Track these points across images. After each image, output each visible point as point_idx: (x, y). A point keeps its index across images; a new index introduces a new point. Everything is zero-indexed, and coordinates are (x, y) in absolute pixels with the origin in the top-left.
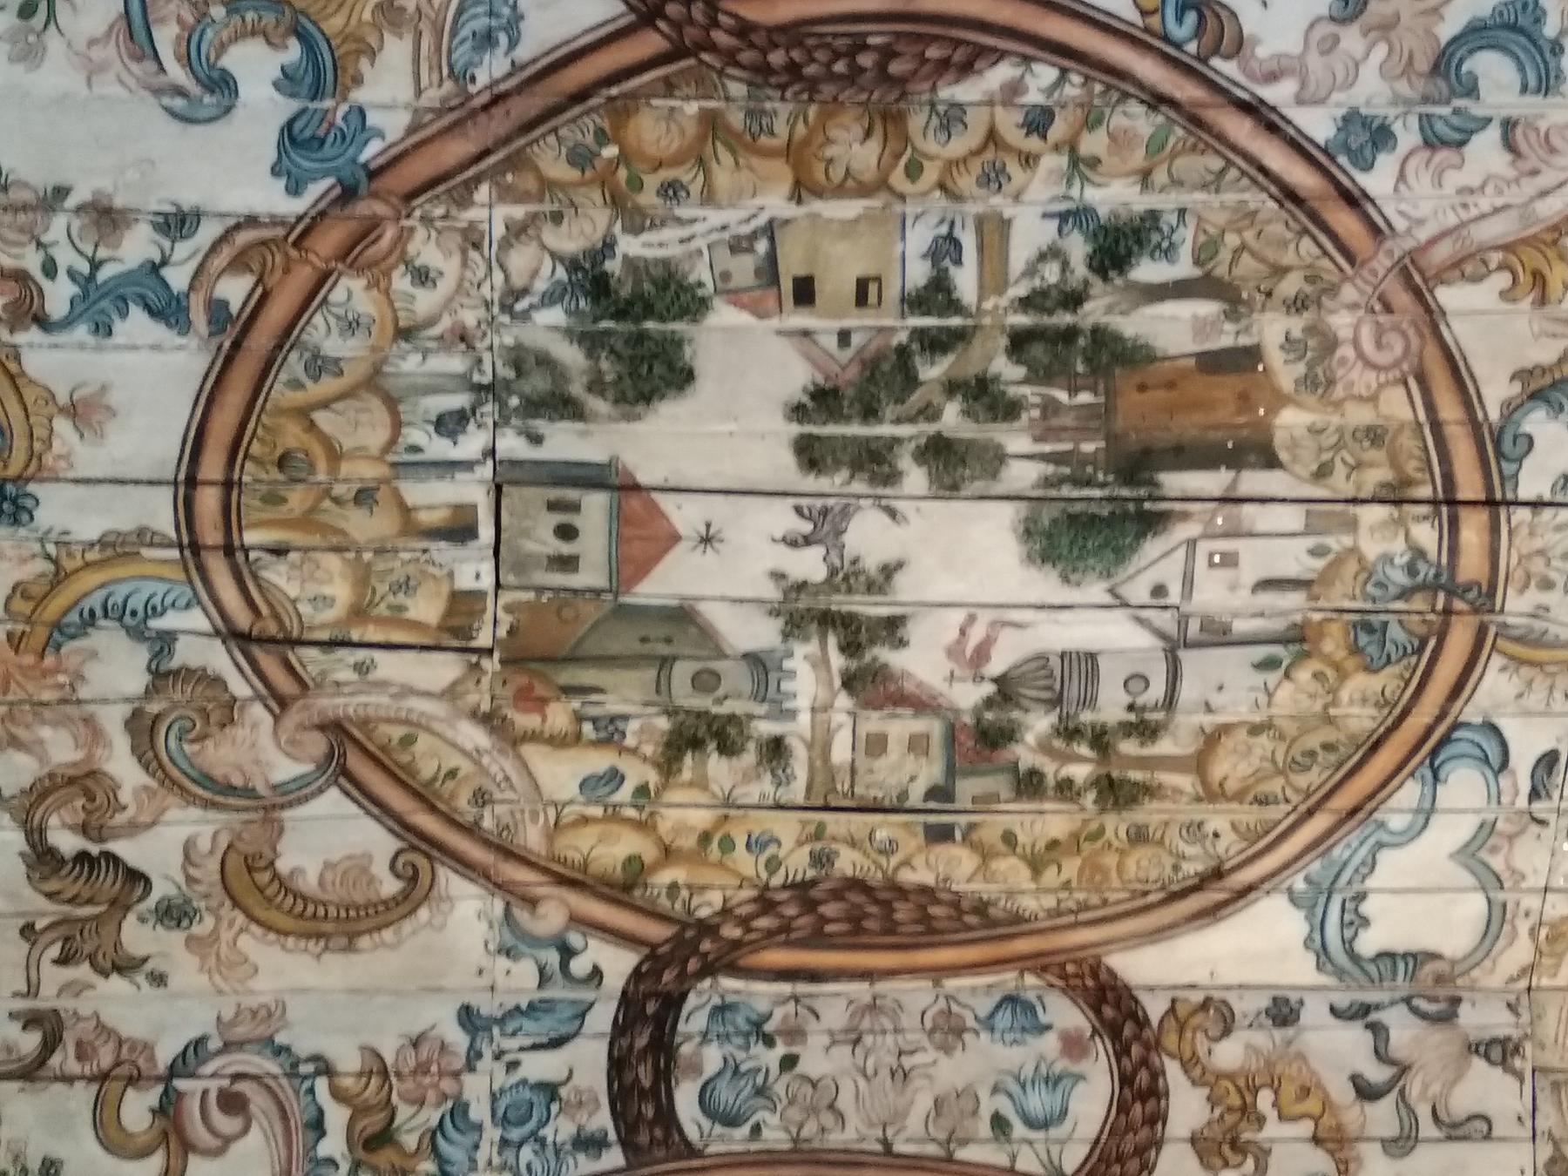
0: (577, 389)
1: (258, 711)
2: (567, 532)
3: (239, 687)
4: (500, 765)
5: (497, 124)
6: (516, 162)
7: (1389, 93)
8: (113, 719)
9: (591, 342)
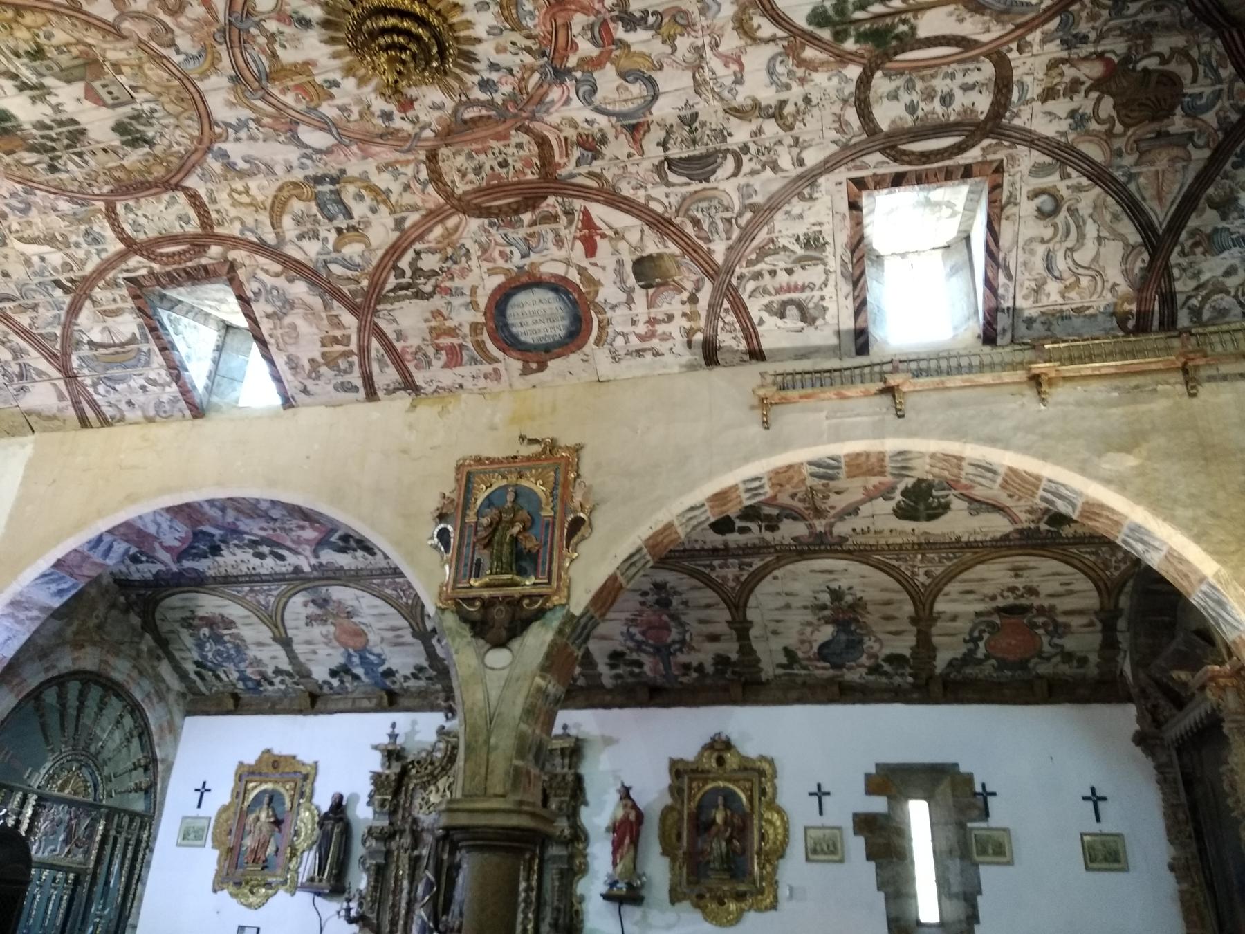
0: (134, 122)
1: (145, 38)
2: (110, 93)
3: (153, 44)
4: (77, 35)
5: (189, 164)
6: (181, 158)
7: (304, 897)
8: (177, 31)
9: (138, 131)
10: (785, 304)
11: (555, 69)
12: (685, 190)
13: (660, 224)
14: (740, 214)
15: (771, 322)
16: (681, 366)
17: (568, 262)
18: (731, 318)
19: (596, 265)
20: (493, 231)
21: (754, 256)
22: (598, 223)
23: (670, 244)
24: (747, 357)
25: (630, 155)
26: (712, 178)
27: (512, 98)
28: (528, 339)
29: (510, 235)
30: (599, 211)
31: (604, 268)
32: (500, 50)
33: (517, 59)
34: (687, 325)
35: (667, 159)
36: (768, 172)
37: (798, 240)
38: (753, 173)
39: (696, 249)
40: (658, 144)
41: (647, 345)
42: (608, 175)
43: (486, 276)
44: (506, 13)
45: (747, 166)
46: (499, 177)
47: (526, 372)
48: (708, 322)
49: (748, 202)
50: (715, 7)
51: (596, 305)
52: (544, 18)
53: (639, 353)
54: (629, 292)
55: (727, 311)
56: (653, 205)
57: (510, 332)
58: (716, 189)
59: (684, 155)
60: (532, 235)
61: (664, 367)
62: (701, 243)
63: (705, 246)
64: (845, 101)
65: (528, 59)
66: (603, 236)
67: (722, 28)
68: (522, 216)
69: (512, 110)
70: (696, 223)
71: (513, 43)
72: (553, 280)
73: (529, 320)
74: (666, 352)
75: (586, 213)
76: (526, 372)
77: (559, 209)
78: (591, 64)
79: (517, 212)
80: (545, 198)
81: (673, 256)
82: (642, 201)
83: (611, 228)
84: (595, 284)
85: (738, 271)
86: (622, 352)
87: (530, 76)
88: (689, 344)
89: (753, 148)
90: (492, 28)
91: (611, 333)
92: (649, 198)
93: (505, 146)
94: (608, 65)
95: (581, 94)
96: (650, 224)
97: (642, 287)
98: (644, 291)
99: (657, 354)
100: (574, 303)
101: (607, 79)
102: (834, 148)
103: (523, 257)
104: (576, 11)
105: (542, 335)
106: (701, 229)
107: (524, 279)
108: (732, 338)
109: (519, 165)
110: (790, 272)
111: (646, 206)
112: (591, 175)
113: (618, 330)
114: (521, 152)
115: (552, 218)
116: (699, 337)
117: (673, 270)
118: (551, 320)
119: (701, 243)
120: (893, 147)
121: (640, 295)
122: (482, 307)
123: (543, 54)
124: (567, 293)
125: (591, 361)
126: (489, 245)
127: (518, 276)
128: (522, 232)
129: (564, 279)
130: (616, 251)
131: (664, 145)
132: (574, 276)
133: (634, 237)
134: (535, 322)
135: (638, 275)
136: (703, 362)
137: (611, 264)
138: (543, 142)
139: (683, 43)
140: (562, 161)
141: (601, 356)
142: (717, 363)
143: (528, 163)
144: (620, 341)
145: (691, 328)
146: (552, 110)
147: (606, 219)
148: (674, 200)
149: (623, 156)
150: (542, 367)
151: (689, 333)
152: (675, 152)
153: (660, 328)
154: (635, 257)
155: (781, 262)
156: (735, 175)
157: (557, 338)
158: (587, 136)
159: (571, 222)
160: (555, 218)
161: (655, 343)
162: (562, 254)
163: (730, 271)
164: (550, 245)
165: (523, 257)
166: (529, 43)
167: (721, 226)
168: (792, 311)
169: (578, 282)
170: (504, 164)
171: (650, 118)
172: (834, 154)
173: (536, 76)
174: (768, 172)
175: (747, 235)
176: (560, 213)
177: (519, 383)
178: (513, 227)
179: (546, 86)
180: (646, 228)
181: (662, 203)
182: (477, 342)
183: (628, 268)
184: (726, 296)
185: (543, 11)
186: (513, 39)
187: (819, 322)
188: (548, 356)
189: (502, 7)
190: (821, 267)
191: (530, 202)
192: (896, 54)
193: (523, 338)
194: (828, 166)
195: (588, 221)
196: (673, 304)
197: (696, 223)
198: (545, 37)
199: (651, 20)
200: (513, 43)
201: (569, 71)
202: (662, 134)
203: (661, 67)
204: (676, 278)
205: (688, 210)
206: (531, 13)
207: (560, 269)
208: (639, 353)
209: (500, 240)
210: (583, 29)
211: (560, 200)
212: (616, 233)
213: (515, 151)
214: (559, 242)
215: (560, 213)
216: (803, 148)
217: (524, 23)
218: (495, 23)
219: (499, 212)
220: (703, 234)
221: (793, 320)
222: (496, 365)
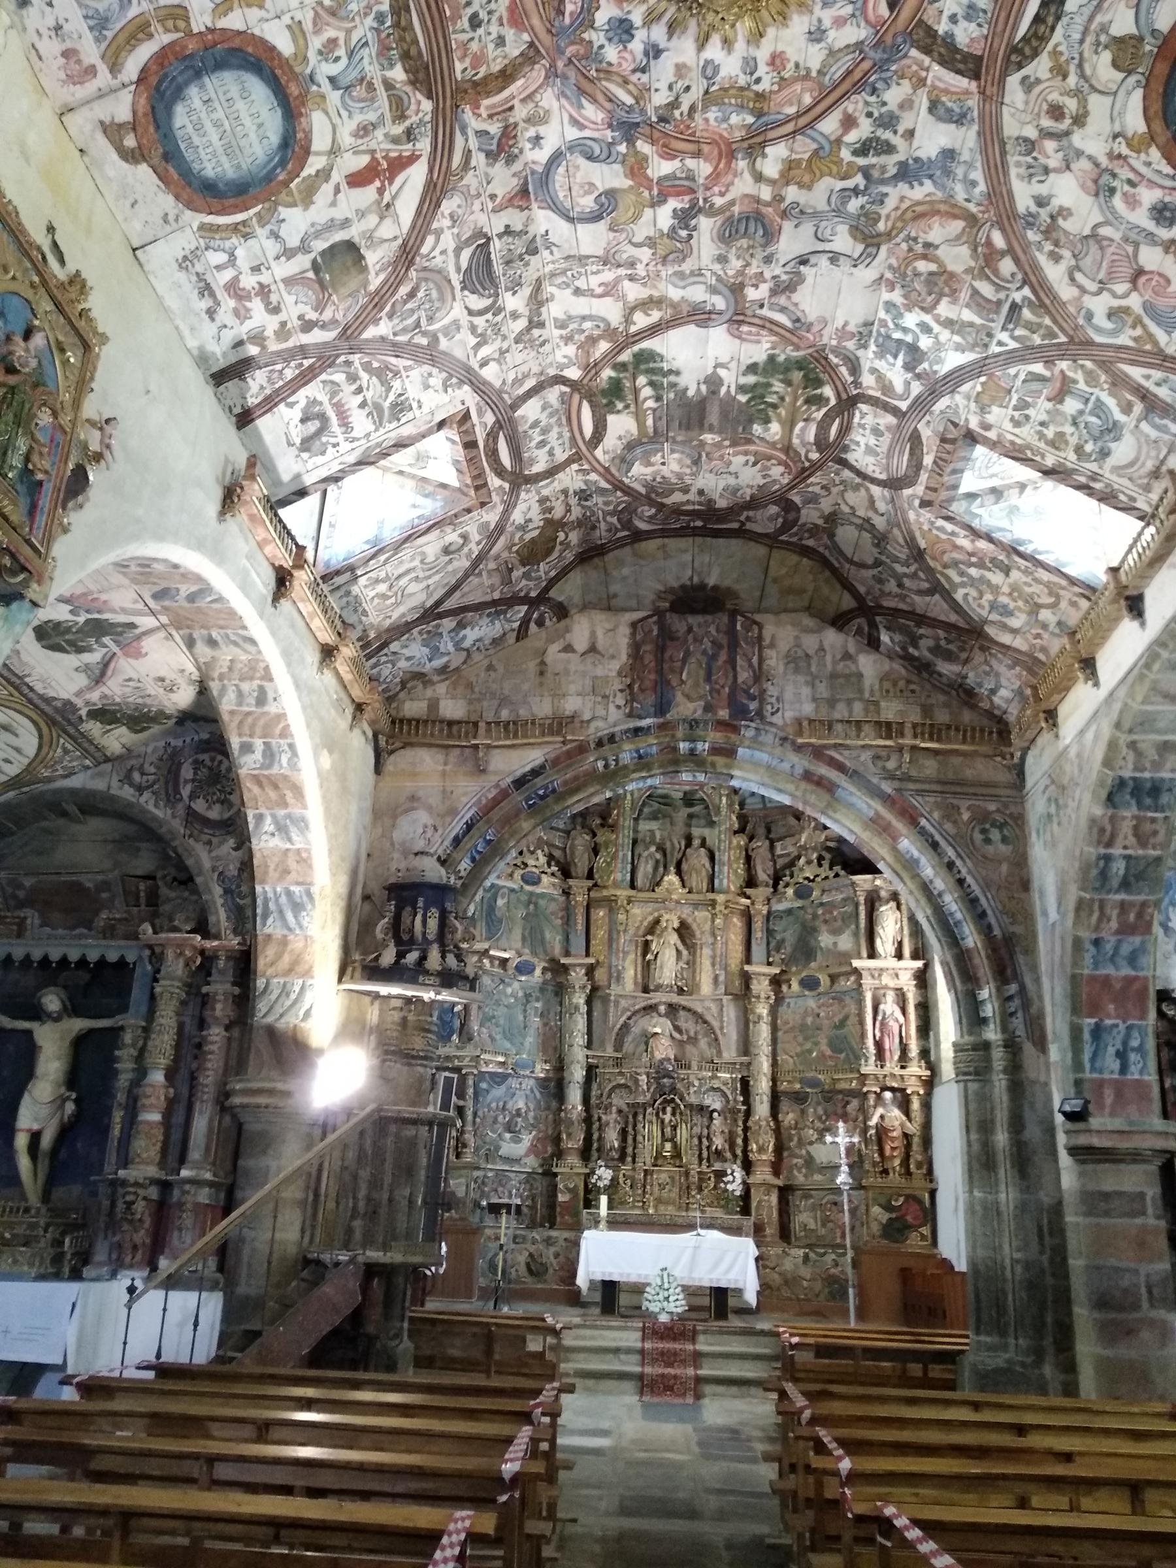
10: (323, 418)
11: (637, 125)
12: (451, 269)
13: (407, 254)
14: (424, 334)
15: (296, 414)
16: (201, 349)
17: (334, 151)
18: (289, 374)
19: (337, 190)
20: (370, 21)
21: (376, 365)
22: (399, 180)
23: (382, 277)
24: (238, 410)
25: (493, 197)
26: (466, 293)
27: (592, 54)
28: (181, 117)
29: (365, 52)
30: (416, 176)
31: (333, 204)
32: (680, 69)
33: (663, 85)
34: (269, 333)
35: (489, 239)
36: (473, 341)
37: (400, 395)
38: (473, 329)
39: (379, 306)
40: (507, 226)
41: (221, 294)
42: (470, 179)
43: (286, 19)
44: (732, 92)
45: (480, 321)
46: (457, 17)
47: (112, 131)
48: (278, 353)
49: (440, 335)
50: (682, 284)
51: (273, 210)
52: (714, 133)
53: (206, 290)
54: (304, 248)
55: (301, 365)
56: (430, 240)
57: (187, 83)
58: (454, 299)
59: (493, 256)
60: (371, 87)
61: (192, 329)
62: (388, 308)
63: (383, 314)
64: (542, 373)
65: (661, 98)
66: (381, 191)
67: (655, 287)
68: (399, 68)
69: (571, 50)
70: (412, 295)
71: (688, 88)
72: (300, 135)
73: (220, 114)
74: (218, 323)
75: (413, 159)
76: (112, 131)
77: (414, 119)
78: (636, 168)
79: (405, 56)
80: (429, 97)
81: (366, 284)
82: (435, 225)
83: (394, 198)
84: (307, 198)
85: (356, 358)
86: (199, 268)
87: (630, 93)
88: (239, 344)
89: (499, 318)
90: (716, 69)
91: (228, 244)
92: (438, 233)
93: (500, 19)
94: (631, 183)
95: (589, 143)
96: (404, 244)
97: (314, 262)
98: (308, 265)
99: (211, 313)
100: (269, 178)
101: (611, 177)
102: (497, 384)
103: (332, 80)
104: (716, 168)
105: (196, 140)
106: (405, 302)
107: (293, 90)
108: (257, 385)
109: (474, 46)
110: (363, 405)
111: (428, 231)
112: (468, 154)
113: (239, 253)
114: (491, 46)
115: (399, 111)
116: (253, 350)
117: (344, 291)
118: (228, 150)
119: (388, 308)
120: (501, 427)
121: (302, 262)
122: (222, 23)
123: (662, 120)
124: (283, 163)
125: (168, 229)
126: (342, 19)
127: (295, 76)
128: (372, 69)
129: (307, 152)
130: (361, 214)
131: (508, 231)
132: (314, 164)
133: (387, 230)
134: (217, 124)
135: (331, 252)
136: (214, 369)
137: (341, 212)
138: (506, 76)
139: (645, 254)
140: (484, 113)
141: (185, 240)
142: (218, 384)
143: (478, 60)
144: (220, 258)
145: (264, 339)
146: (563, 101)
147: (406, 188)
148: (438, 261)
149: (491, 189)
150: (131, 156)
151: (258, 338)
152: (497, 246)
153: (256, 305)
154: (356, 240)
155: (373, 390)
156: (471, 313)
157: (196, 167)
158: (515, 136)
159: (395, 140)
160: (400, 115)
161: (228, 303)
162: (346, 140)
163: (352, 350)
164: (359, 118)
165: (332, 80)
166: (685, 108)
167: (410, 321)
168: (313, 426)
169: (304, 174)
170: (475, 22)
171: (534, 206)
172: (489, 384)
173: (629, 100)
174: (473, 341)
175: (397, 349)
176: (408, 123)
177: (82, 123)
178: (380, 54)
179: (608, 105)
180: (400, 241)
181: (433, 249)
182: (148, 24)
183: (339, 236)
184: (319, 359)
185: (725, 134)
186: (693, 89)
187: (305, 455)
188: (156, 161)
189: (742, 89)
190: (373, 428)
191: (421, 75)
192: (590, 402)
193: (180, 110)
194: (480, 387)
195: (399, 165)
196: (295, 306)
197: (412, 295)
198: (688, 127)
199: (684, 233)
200: (688, 88)
201: (631, 142)
202: (518, 227)
203: (611, 229)
204: (334, 297)
205: (426, 280)
206: (726, 119)
207: (320, 141)
208: (206, 290)
209: (355, 37)
210: (689, 170)
211: (428, 118)
212: (388, 206)
213: (494, 35)
214: (364, 130)
215: (408, 123)
216: (498, 361)
217: (714, 108)
218: (723, 73)
219: (402, 27)
220: (398, 307)
221: (297, 433)
222: (103, 69)
